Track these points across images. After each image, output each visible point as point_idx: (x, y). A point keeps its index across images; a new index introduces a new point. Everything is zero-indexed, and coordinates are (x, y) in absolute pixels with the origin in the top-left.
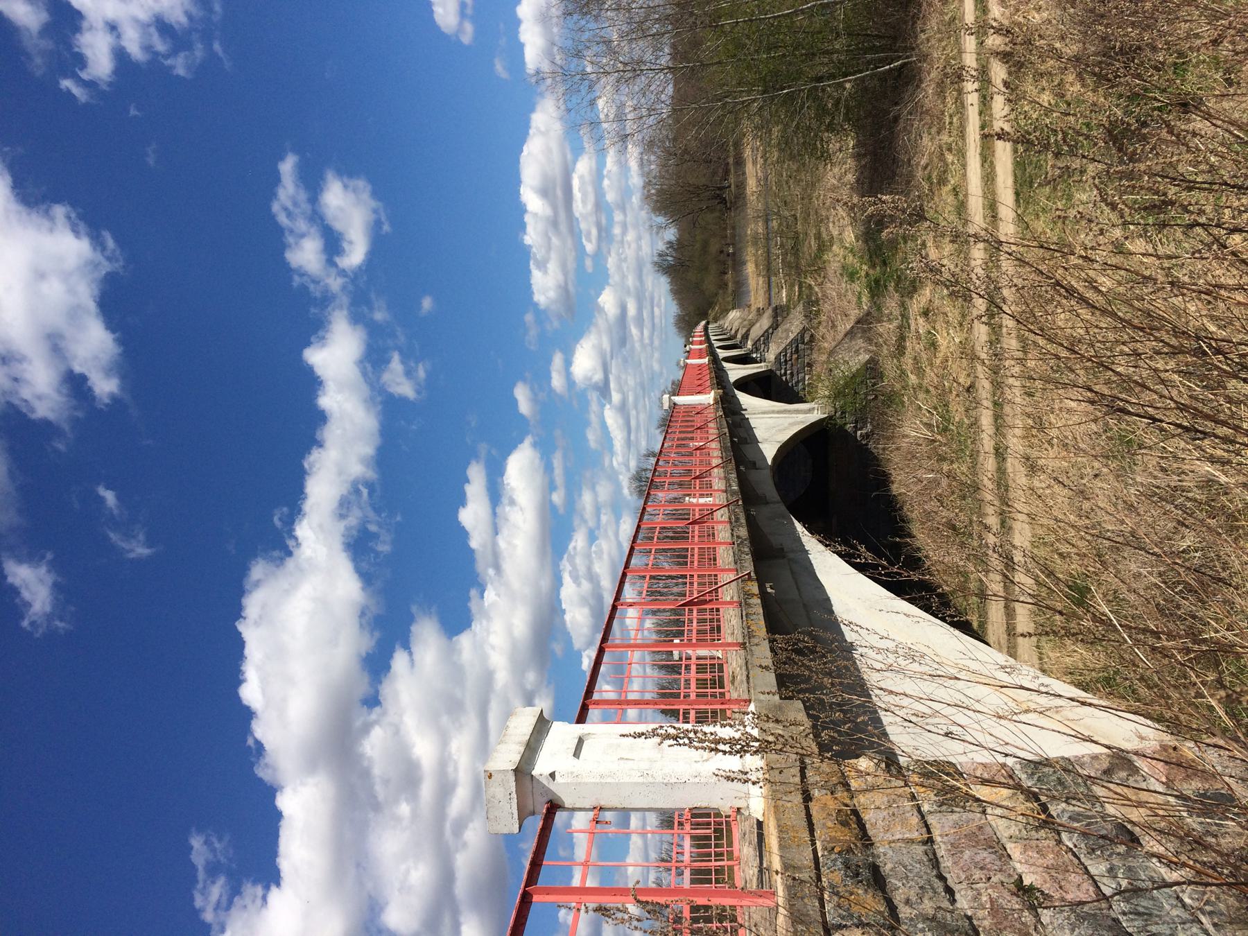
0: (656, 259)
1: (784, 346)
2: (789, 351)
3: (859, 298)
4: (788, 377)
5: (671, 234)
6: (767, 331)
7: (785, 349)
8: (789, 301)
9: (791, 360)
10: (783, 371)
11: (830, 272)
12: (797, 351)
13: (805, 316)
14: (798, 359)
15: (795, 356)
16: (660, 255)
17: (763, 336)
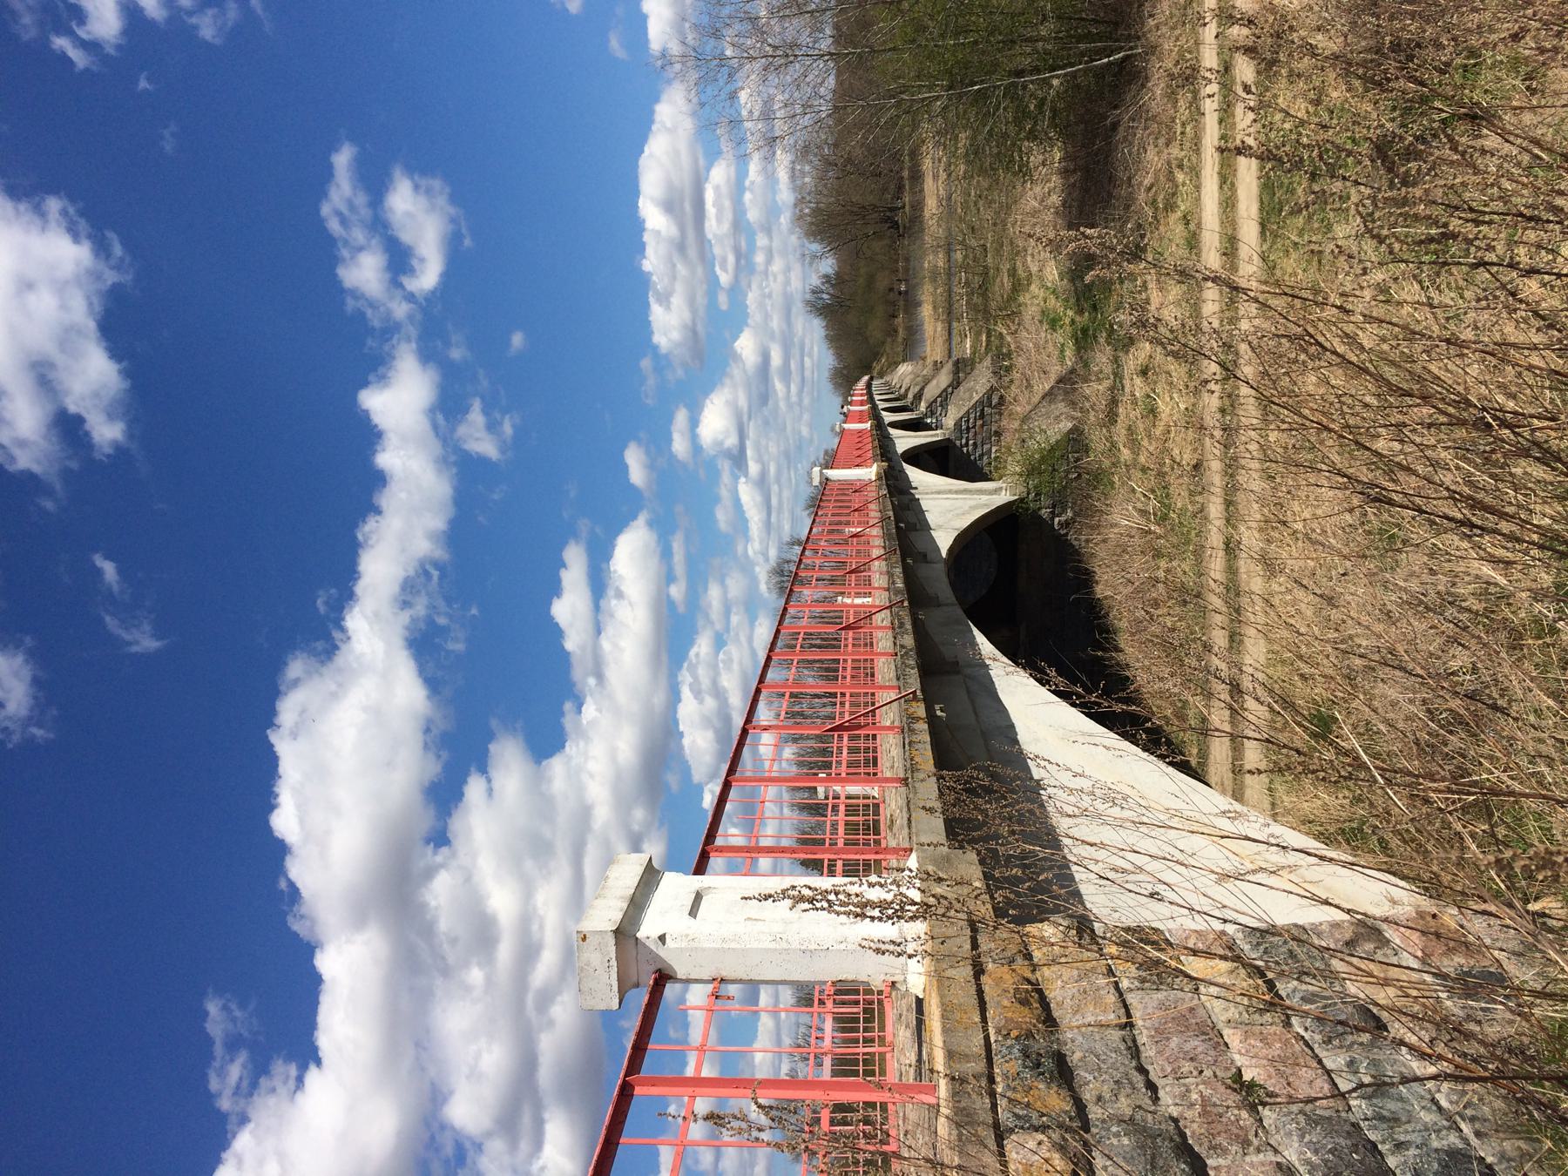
0: (808, 296)
2: (972, 416)
3: (1062, 351)
6: (945, 390)
7: (968, 412)
8: (974, 353)
10: (964, 441)
11: (1027, 317)
12: (982, 416)
13: (994, 373)
14: (982, 426)
15: (979, 422)
16: (814, 292)
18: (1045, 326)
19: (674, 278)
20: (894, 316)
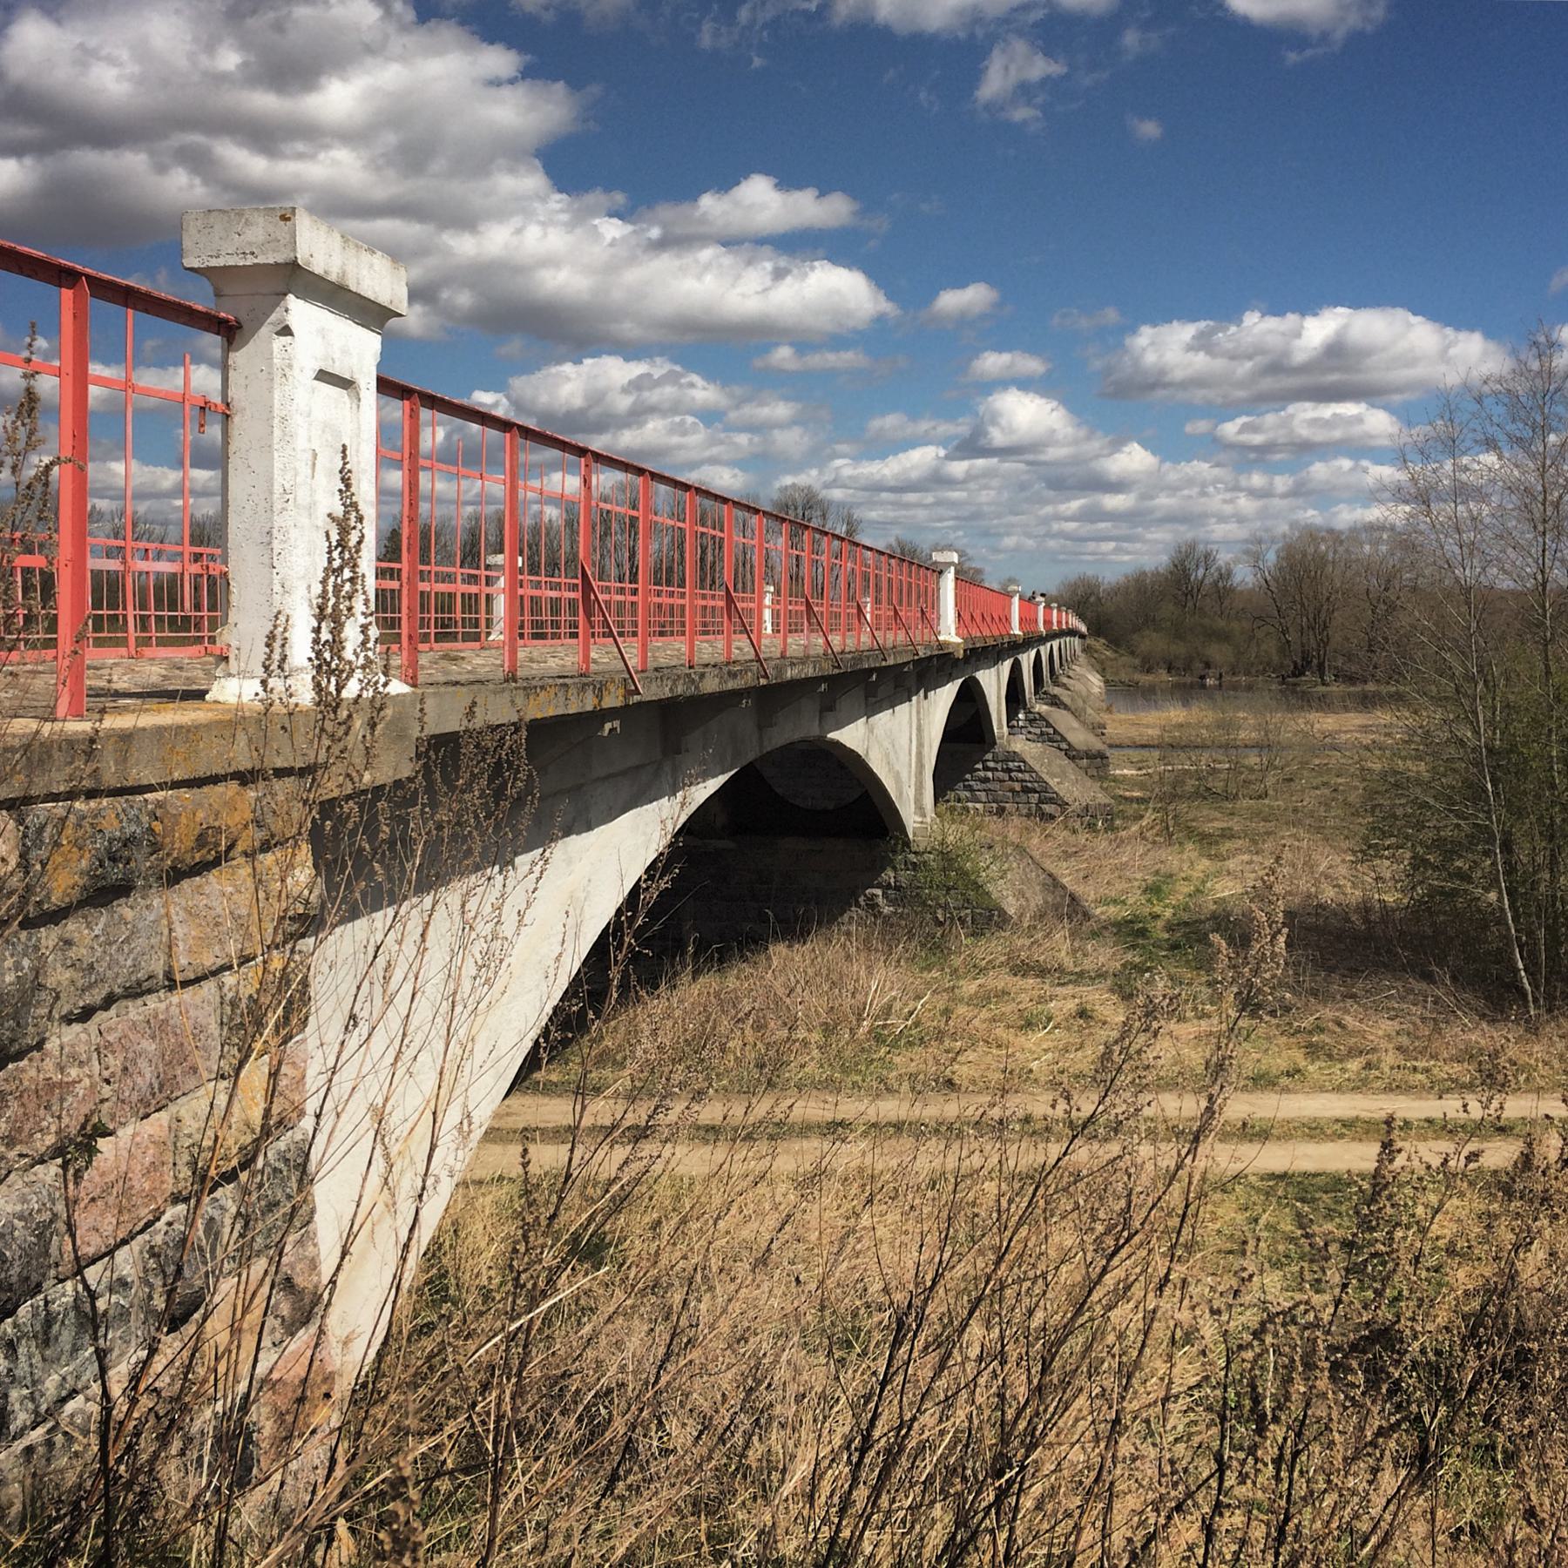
1: (1037, 768)
2: (1027, 776)
4: (982, 774)
5: (1244, 576)
6: (1064, 739)
7: (1032, 770)
8: (1115, 779)
9: (1011, 779)
10: (991, 764)
11: (1163, 854)
12: (1026, 790)
14: (1012, 790)
15: (1017, 786)
16: (1207, 556)
17: (1055, 731)
18: (1150, 879)
19: (1233, 357)
20: (1169, 670)
